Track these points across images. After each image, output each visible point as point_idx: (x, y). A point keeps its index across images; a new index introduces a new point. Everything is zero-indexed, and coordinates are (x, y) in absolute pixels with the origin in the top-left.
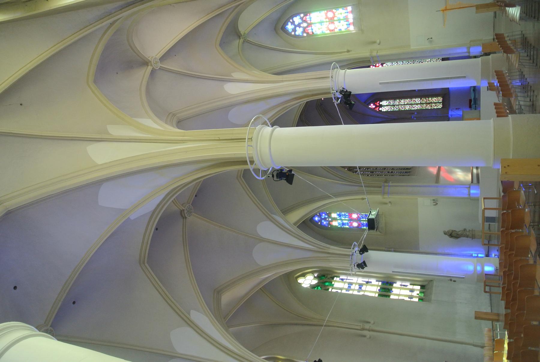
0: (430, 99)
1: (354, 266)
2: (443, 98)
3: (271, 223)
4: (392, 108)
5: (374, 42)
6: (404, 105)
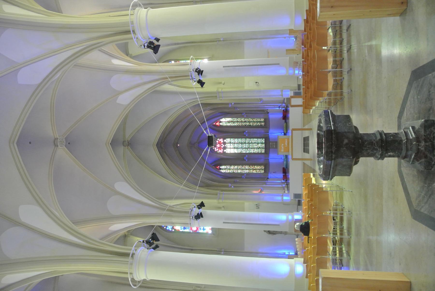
0: (256, 167)
1: (193, 217)
3: (127, 184)
4: (229, 171)
5: (221, 83)
6: (237, 169)
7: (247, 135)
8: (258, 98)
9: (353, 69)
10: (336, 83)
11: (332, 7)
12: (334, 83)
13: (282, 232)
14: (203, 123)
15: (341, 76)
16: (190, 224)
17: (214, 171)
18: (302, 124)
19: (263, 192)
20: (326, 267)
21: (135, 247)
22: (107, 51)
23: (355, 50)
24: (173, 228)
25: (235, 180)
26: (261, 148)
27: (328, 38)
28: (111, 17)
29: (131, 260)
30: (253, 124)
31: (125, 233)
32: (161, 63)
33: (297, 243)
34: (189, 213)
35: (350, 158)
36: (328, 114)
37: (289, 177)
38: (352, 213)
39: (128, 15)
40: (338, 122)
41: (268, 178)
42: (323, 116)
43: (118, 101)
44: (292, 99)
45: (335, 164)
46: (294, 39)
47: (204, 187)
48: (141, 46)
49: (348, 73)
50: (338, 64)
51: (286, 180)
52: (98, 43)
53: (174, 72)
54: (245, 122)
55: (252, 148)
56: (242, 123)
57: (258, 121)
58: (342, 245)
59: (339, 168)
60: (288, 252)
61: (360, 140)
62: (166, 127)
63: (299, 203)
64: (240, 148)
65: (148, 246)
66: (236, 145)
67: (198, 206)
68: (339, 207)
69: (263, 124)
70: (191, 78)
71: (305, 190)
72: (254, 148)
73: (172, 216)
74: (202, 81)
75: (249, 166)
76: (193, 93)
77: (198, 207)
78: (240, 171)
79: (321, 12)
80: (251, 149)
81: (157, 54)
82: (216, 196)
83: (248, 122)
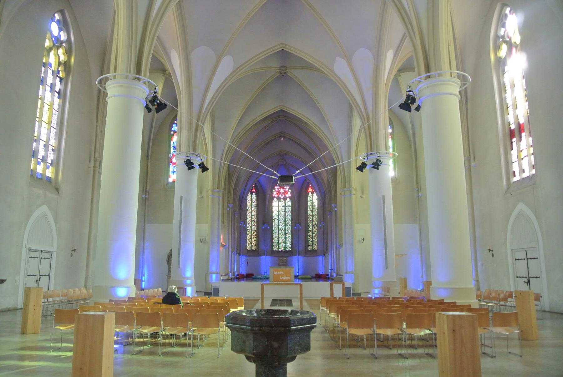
0: (255, 239)
1: (188, 157)
2: (255, 250)
4: (249, 204)
5: (363, 193)
6: (252, 215)
7: (295, 227)
8: (343, 242)
9: (376, 360)
10: (359, 339)
11: (454, 331)
12: (359, 337)
13: (171, 271)
14: (310, 169)
15: (368, 346)
16: (180, 154)
17: (249, 185)
18: (309, 298)
19: (222, 248)
20: (118, 323)
21: (149, 82)
22: (404, 45)
23: (400, 364)
24: (175, 132)
25: (238, 212)
26: (279, 246)
27: (417, 329)
28: (447, 46)
29: (131, 77)
30: (310, 235)
31: (168, 70)
32: (389, 114)
33: (156, 290)
34: (193, 152)
35: (253, 350)
36: (312, 322)
37: (241, 281)
38: (191, 357)
39: (451, 69)
40: (300, 335)
41: (240, 255)
42: (308, 316)
43: (338, 59)
44: (341, 284)
45: (246, 331)
46: (420, 289)
47: (227, 171)
48: (410, 87)
49: (371, 354)
50: (384, 343)
51: (237, 278)
52: (413, 31)
53: (377, 132)
54: (313, 225)
55: (278, 234)
56: (311, 222)
57: (314, 242)
58: (151, 345)
59: (242, 336)
60: (145, 280)
61: (277, 364)
62: (306, 122)
63: (207, 294)
64: (279, 218)
65: (150, 99)
66: (282, 213)
67: (203, 163)
68: (198, 342)
69: (310, 248)
70: (369, 153)
71: (221, 299)
72: (279, 237)
73: (190, 130)
74: (365, 168)
75: (255, 231)
76: (349, 157)
77: (201, 164)
78: (249, 219)
79: (448, 316)
80: (277, 233)
81: (399, 108)
82: (217, 188)
83: (313, 229)
